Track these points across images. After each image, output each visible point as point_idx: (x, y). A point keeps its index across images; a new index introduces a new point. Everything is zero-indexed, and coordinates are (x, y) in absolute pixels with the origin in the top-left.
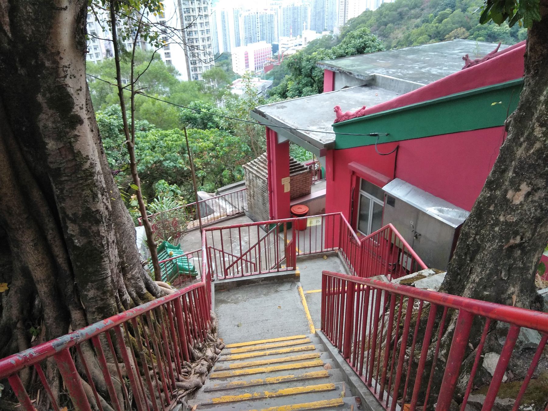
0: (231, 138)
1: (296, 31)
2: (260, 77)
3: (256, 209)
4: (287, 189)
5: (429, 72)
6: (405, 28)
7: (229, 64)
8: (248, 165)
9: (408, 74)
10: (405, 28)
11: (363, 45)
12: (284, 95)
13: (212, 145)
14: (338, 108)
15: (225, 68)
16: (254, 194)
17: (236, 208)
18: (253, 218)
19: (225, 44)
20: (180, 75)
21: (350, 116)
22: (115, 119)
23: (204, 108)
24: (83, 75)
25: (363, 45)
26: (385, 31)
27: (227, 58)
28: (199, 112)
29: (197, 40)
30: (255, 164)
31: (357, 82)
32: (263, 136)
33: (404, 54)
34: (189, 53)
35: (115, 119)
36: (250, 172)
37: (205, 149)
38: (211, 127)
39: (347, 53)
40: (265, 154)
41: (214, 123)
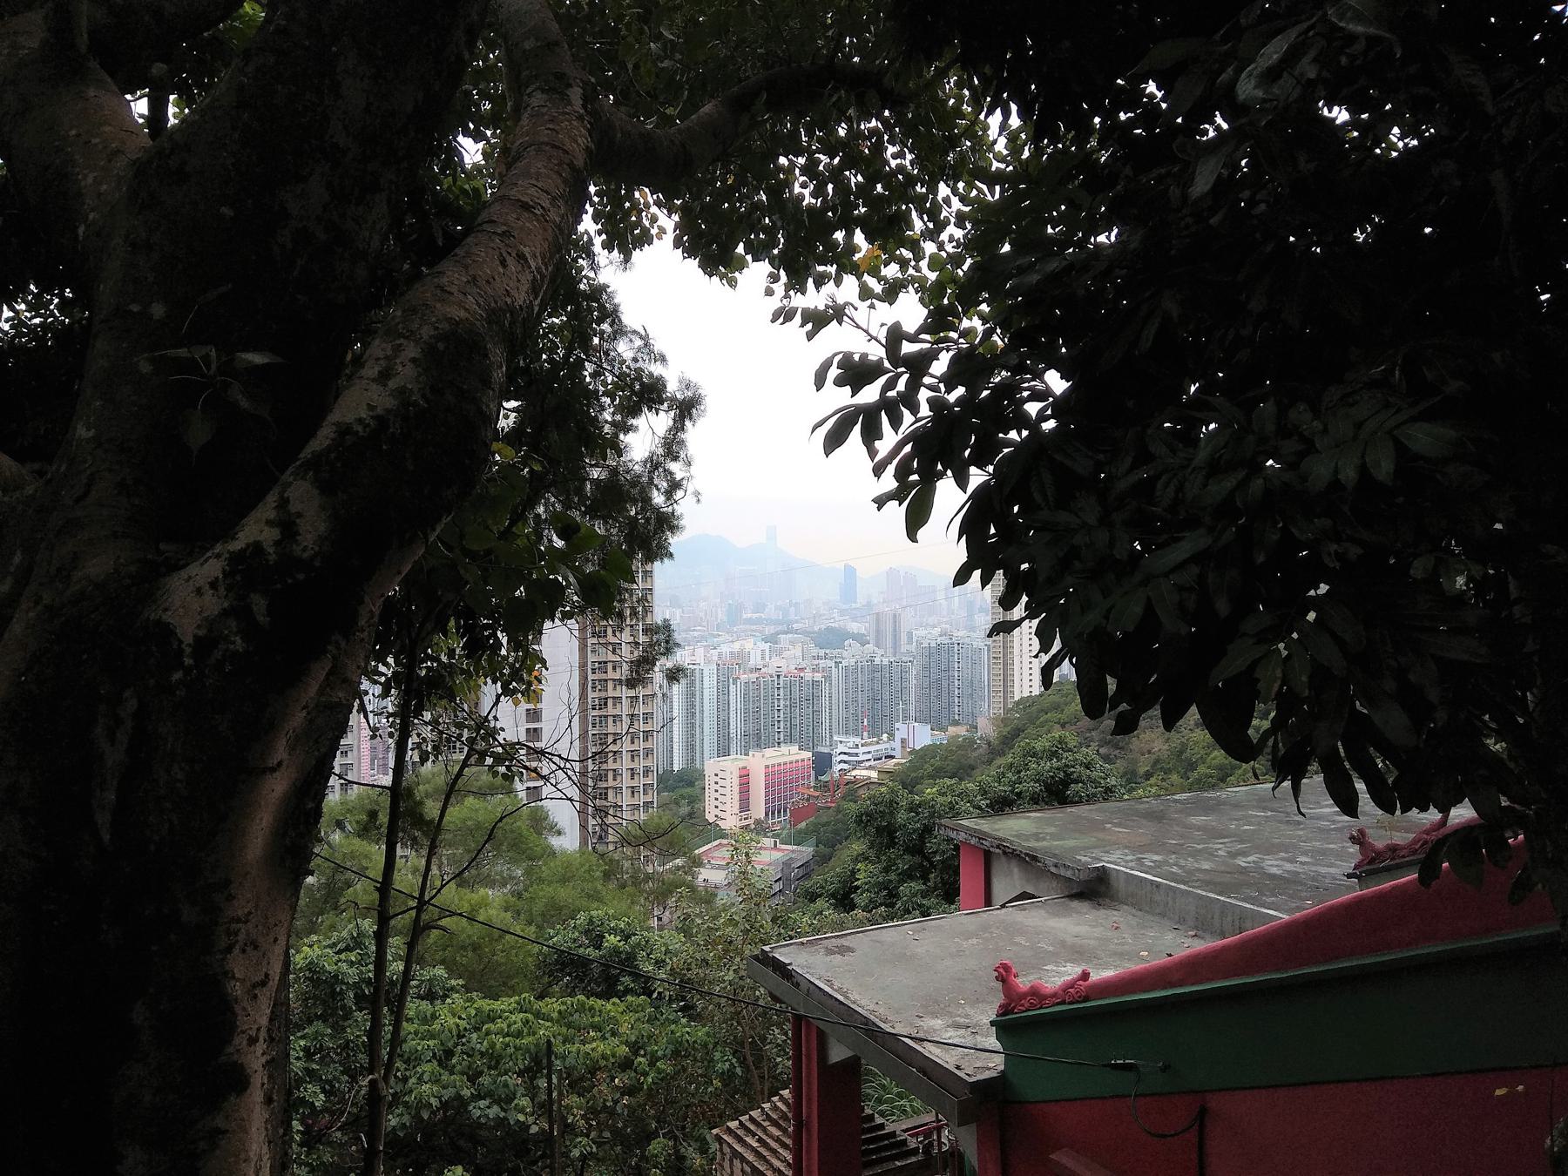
0: (685, 1029)
1: (879, 724)
2: (777, 836)
5: (1258, 867)
7: (696, 799)
8: (730, 1131)
9: (1199, 870)
11: (1062, 775)
12: (844, 900)
14: (1006, 968)
15: (685, 810)
19: (690, 747)
20: (559, 833)
21: (1045, 997)
22: (352, 964)
23: (613, 931)
24: (282, 941)
25: (1062, 775)
27: (691, 784)
28: (597, 942)
29: (618, 790)
30: (752, 1127)
31: (1054, 884)
32: (779, 1025)
33: (1181, 812)
34: (591, 822)
35: (352, 964)
36: (735, 1154)
38: (627, 991)
39: (1019, 795)
40: (786, 1093)
41: (636, 976)
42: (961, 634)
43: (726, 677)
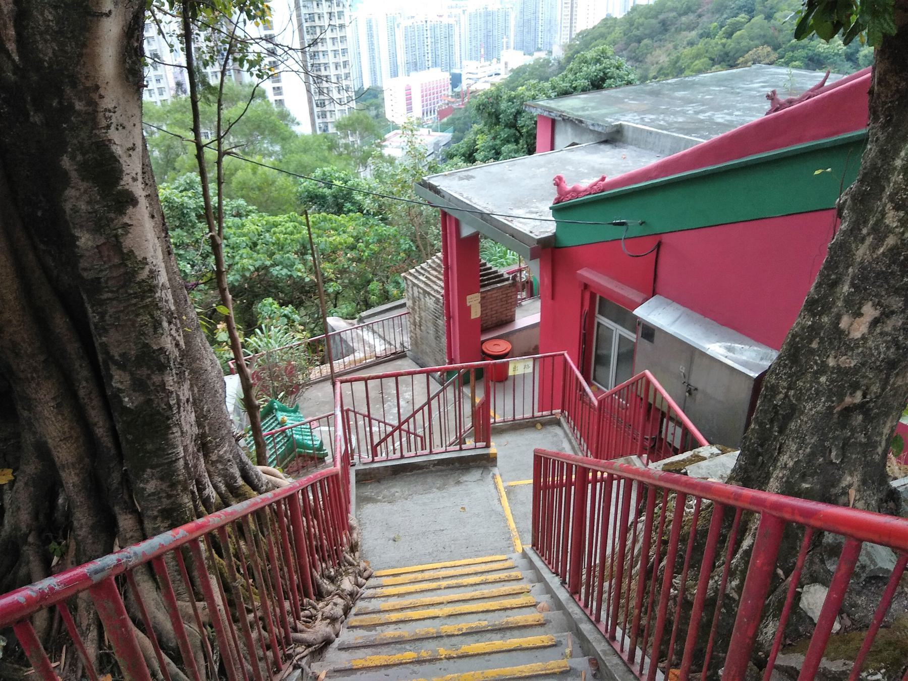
0: (383, 229)
1: (490, 51)
2: (430, 127)
3: (424, 347)
4: (476, 313)
5: (710, 119)
6: (671, 46)
7: (379, 106)
8: (411, 274)
9: (676, 122)
10: (671, 46)
11: (601, 74)
12: (470, 157)
13: (351, 240)
14: (560, 178)
15: (373, 113)
16: (420, 322)
17: (390, 344)
18: (419, 362)
19: (373, 72)
20: (298, 124)
21: (580, 192)
22: (190, 198)
23: (338, 179)
24: (138, 125)
25: (601, 74)
26: (637, 51)
27: (376, 96)
28: (329, 185)
29: (326, 66)
30: (422, 271)
31: (591, 136)
32: (435, 225)
33: (670, 90)
34: (312, 87)
35: (190, 198)
36: (414, 284)
37: (340, 247)
38: (349, 211)
39: (575, 88)
40: (439, 254)
41: (354, 203)
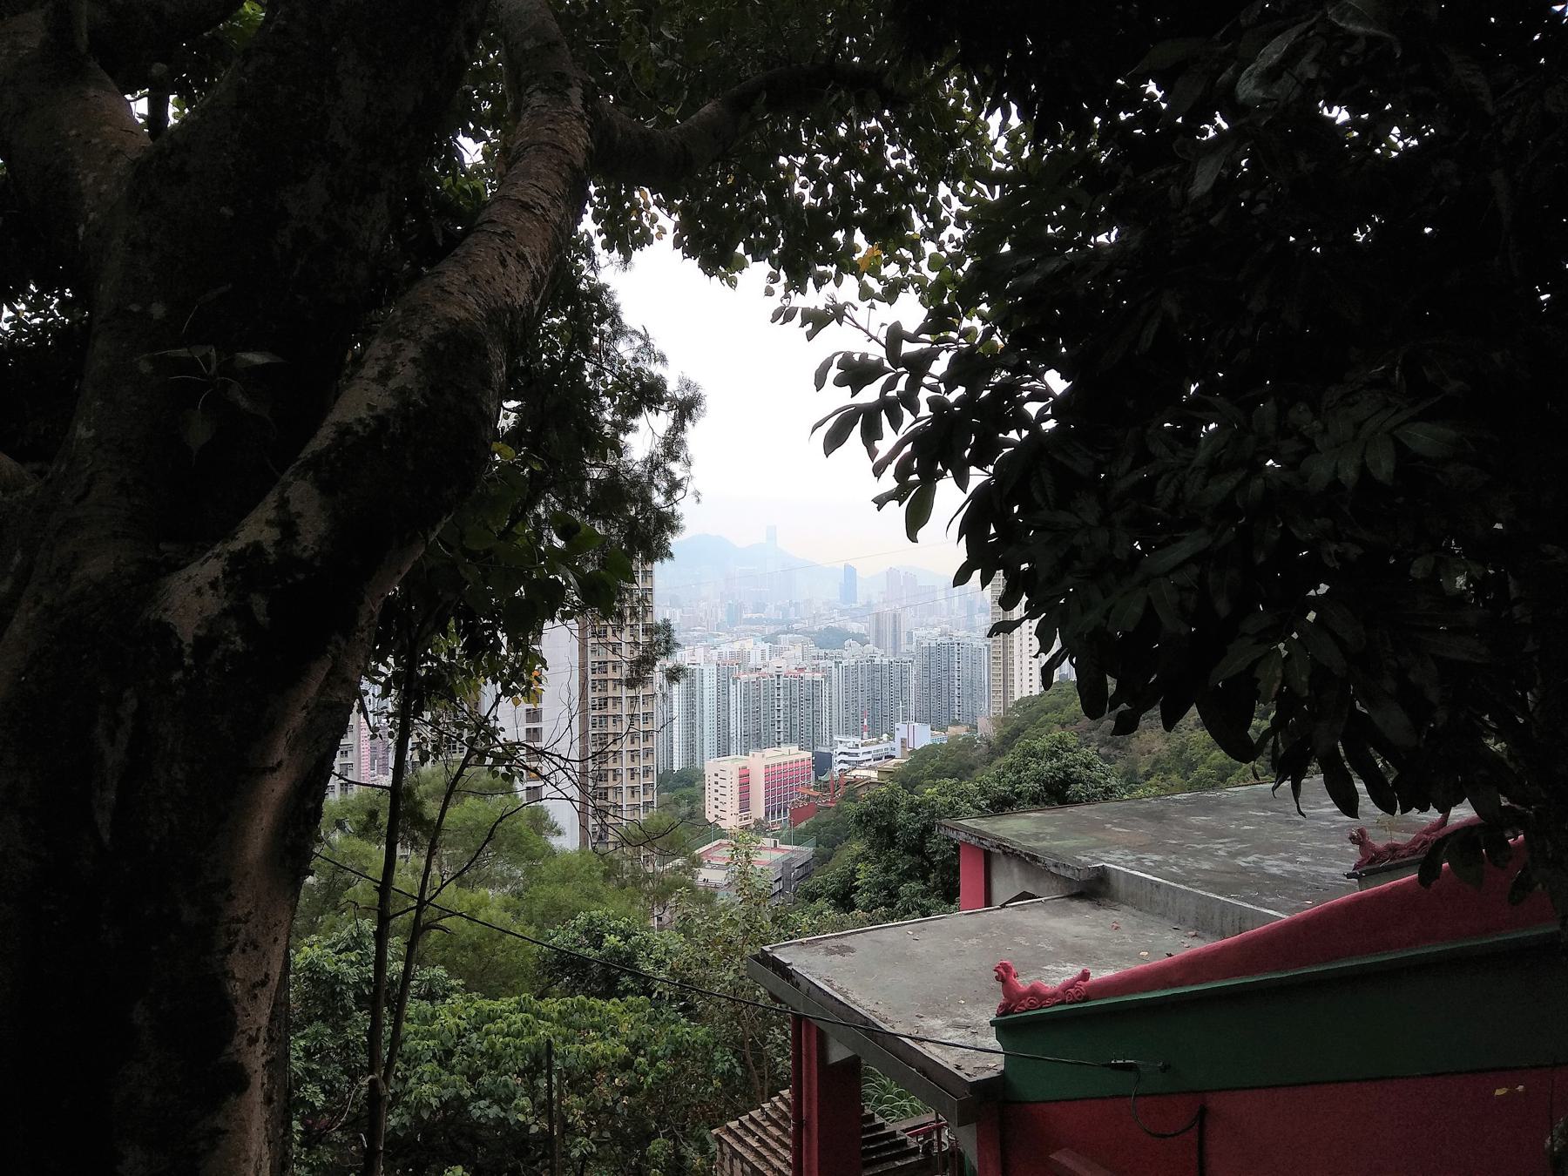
0: (685, 1029)
1: (879, 724)
2: (777, 836)
5: (1258, 867)
7: (696, 799)
8: (730, 1131)
9: (1199, 870)
11: (1062, 775)
12: (844, 900)
14: (1006, 968)
15: (685, 810)
19: (690, 747)
20: (559, 833)
21: (1045, 997)
22: (352, 964)
23: (613, 931)
24: (282, 941)
25: (1062, 775)
27: (691, 784)
28: (597, 942)
29: (618, 790)
30: (752, 1127)
31: (1054, 884)
32: (779, 1025)
33: (1181, 812)
34: (591, 822)
35: (352, 964)
36: (735, 1154)
38: (627, 991)
39: (1019, 795)
40: (786, 1093)
41: (636, 976)
42: (961, 634)
43: (726, 677)
